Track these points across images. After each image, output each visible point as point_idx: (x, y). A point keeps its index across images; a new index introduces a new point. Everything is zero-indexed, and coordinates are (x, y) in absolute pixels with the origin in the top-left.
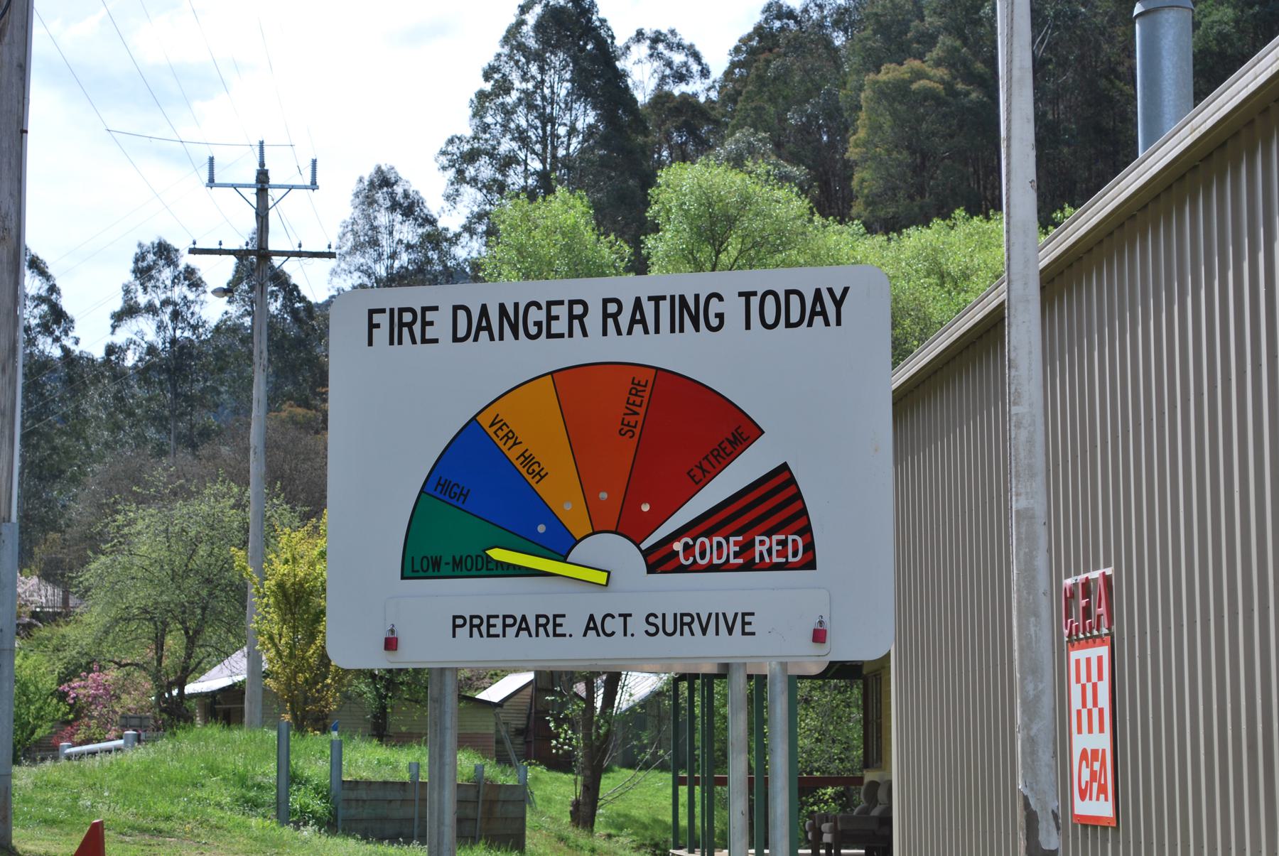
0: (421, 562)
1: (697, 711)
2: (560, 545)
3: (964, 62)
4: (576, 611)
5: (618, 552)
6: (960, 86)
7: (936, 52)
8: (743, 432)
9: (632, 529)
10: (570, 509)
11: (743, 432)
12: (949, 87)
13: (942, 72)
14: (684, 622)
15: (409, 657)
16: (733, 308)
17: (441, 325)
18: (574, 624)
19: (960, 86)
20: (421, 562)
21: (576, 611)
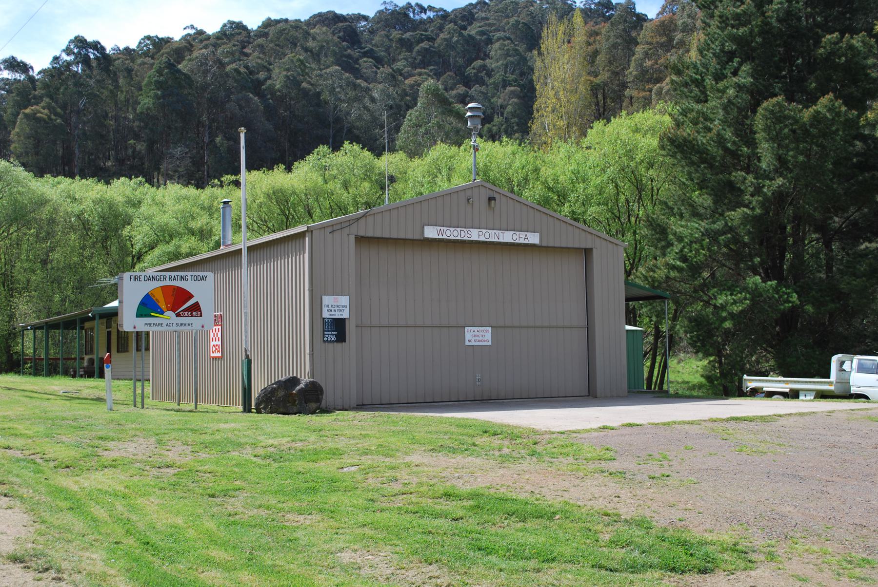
0: (139, 315)
1: (654, 379)
2: (162, 313)
3: (53, 108)
4: (165, 322)
5: (170, 314)
6: (53, 117)
7: (43, 104)
8: (191, 296)
9: (174, 310)
10: (163, 307)
11: (191, 296)
12: (49, 117)
13: (46, 111)
14: (182, 324)
15: (138, 329)
16: (190, 278)
17: (142, 278)
18: (164, 325)
19: (53, 117)
20: (139, 315)
21: (165, 322)
